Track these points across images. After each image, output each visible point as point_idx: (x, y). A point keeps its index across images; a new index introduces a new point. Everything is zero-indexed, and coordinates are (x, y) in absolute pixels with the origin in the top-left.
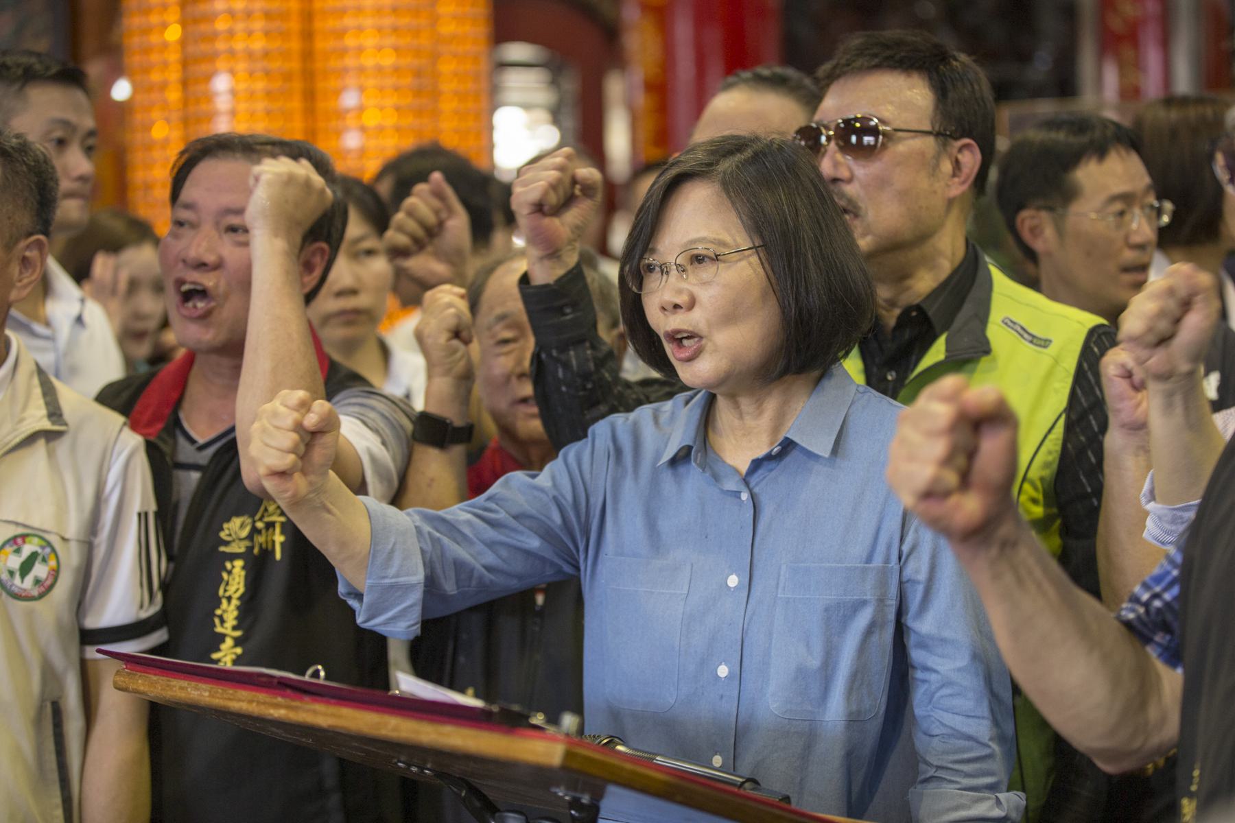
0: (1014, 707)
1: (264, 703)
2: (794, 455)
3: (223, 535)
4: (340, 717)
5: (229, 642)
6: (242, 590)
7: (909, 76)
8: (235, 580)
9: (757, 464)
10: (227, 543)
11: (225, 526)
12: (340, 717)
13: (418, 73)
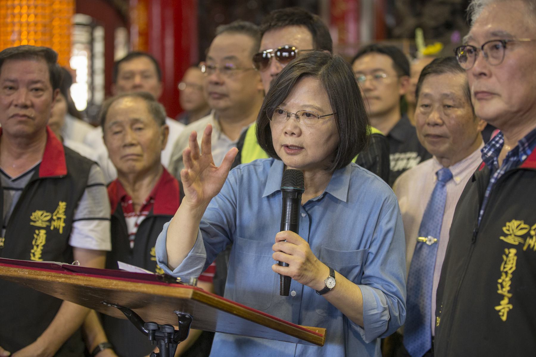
1: (54, 276)
3: (504, 229)
4: (90, 281)
6: (514, 269)
7: (300, 27)
8: (41, 238)
10: (506, 235)
11: (508, 224)
12: (90, 281)
13: (45, 26)
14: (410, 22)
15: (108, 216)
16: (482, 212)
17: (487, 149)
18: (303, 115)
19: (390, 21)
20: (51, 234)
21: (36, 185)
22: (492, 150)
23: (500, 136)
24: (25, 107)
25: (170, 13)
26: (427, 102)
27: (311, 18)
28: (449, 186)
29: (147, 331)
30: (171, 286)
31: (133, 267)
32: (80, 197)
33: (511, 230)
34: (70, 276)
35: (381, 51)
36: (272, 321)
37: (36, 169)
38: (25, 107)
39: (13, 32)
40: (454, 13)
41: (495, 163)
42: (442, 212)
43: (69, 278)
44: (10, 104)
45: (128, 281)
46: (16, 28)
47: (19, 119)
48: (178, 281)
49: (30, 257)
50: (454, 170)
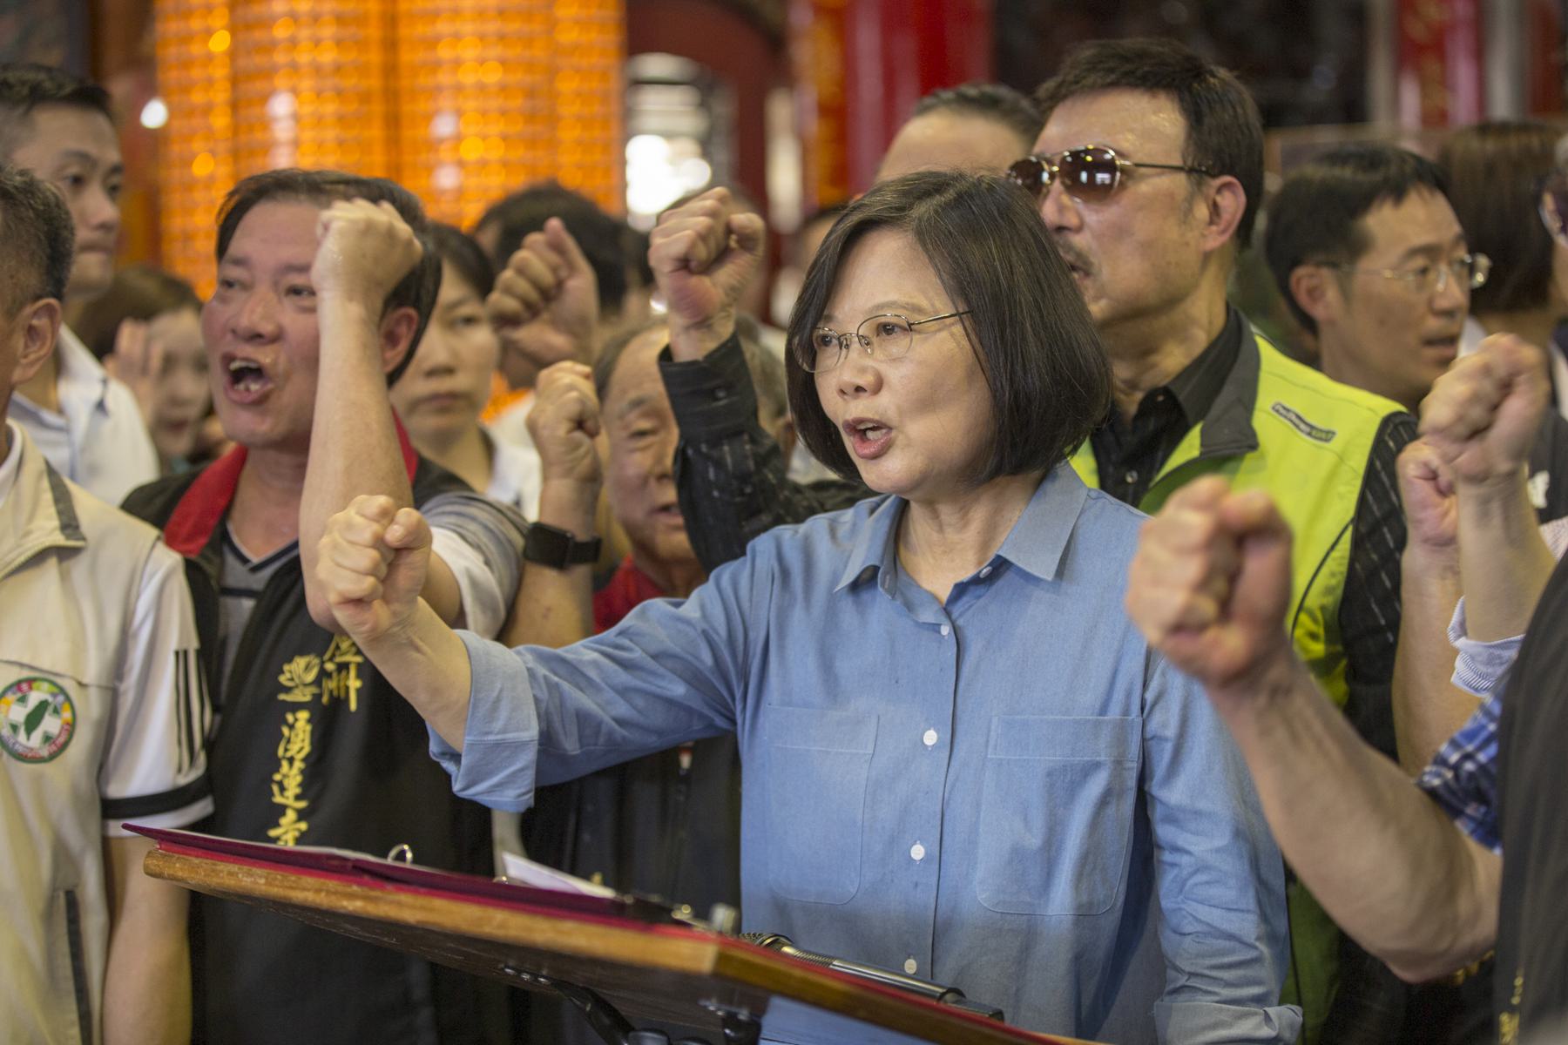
0: (1287, 897)
2: (1008, 577)
3: (283, 679)
5: (291, 815)
6: (307, 749)
7: (1154, 96)
8: (299, 737)
9: (961, 590)
10: (288, 690)
11: (286, 667)
13: (530, 93)
24: (255, 337)
49: (272, 794)
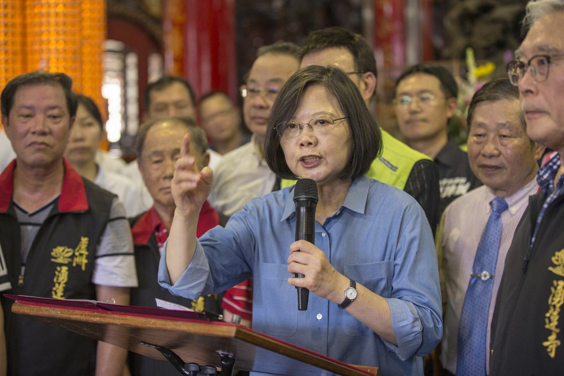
1: (88, 315)
2: (346, 214)
3: (553, 259)
4: (126, 320)
7: (340, 48)
8: (63, 275)
9: (329, 220)
10: (554, 266)
11: (557, 254)
12: (126, 320)
13: (74, 52)
14: (460, 42)
15: (132, 251)
16: (533, 239)
17: (543, 172)
18: (316, 123)
19: (438, 42)
20: (74, 270)
21: (56, 220)
22: (549, 172)
23: (558, 157)
24: (43, 134)
25: (206, 38)
26: (481, 131)
27: (352, 38)
28: (505, 218)
29: (187, 373)
30: (213, 324)
31: (172, 304)
32: (102, 233)
33: (560, 260)
34: (105, 315)
35: (428, 71)
36: (321, 360)
37: (55, 202)
38: (43, 134)
39: (41, 59)
40: (505, 31)
41: (551, 186)
42: (498, 245)
43: (104, 317)
44: (27, 132)
45: (167, 319)
46: (44, 56)
47: (37, 146)
48: (220, 318)
49: (52, 295)
50: (509, 201)
